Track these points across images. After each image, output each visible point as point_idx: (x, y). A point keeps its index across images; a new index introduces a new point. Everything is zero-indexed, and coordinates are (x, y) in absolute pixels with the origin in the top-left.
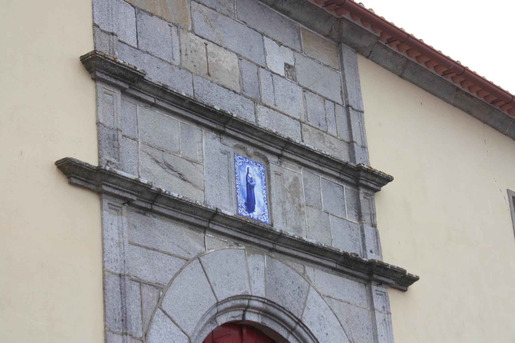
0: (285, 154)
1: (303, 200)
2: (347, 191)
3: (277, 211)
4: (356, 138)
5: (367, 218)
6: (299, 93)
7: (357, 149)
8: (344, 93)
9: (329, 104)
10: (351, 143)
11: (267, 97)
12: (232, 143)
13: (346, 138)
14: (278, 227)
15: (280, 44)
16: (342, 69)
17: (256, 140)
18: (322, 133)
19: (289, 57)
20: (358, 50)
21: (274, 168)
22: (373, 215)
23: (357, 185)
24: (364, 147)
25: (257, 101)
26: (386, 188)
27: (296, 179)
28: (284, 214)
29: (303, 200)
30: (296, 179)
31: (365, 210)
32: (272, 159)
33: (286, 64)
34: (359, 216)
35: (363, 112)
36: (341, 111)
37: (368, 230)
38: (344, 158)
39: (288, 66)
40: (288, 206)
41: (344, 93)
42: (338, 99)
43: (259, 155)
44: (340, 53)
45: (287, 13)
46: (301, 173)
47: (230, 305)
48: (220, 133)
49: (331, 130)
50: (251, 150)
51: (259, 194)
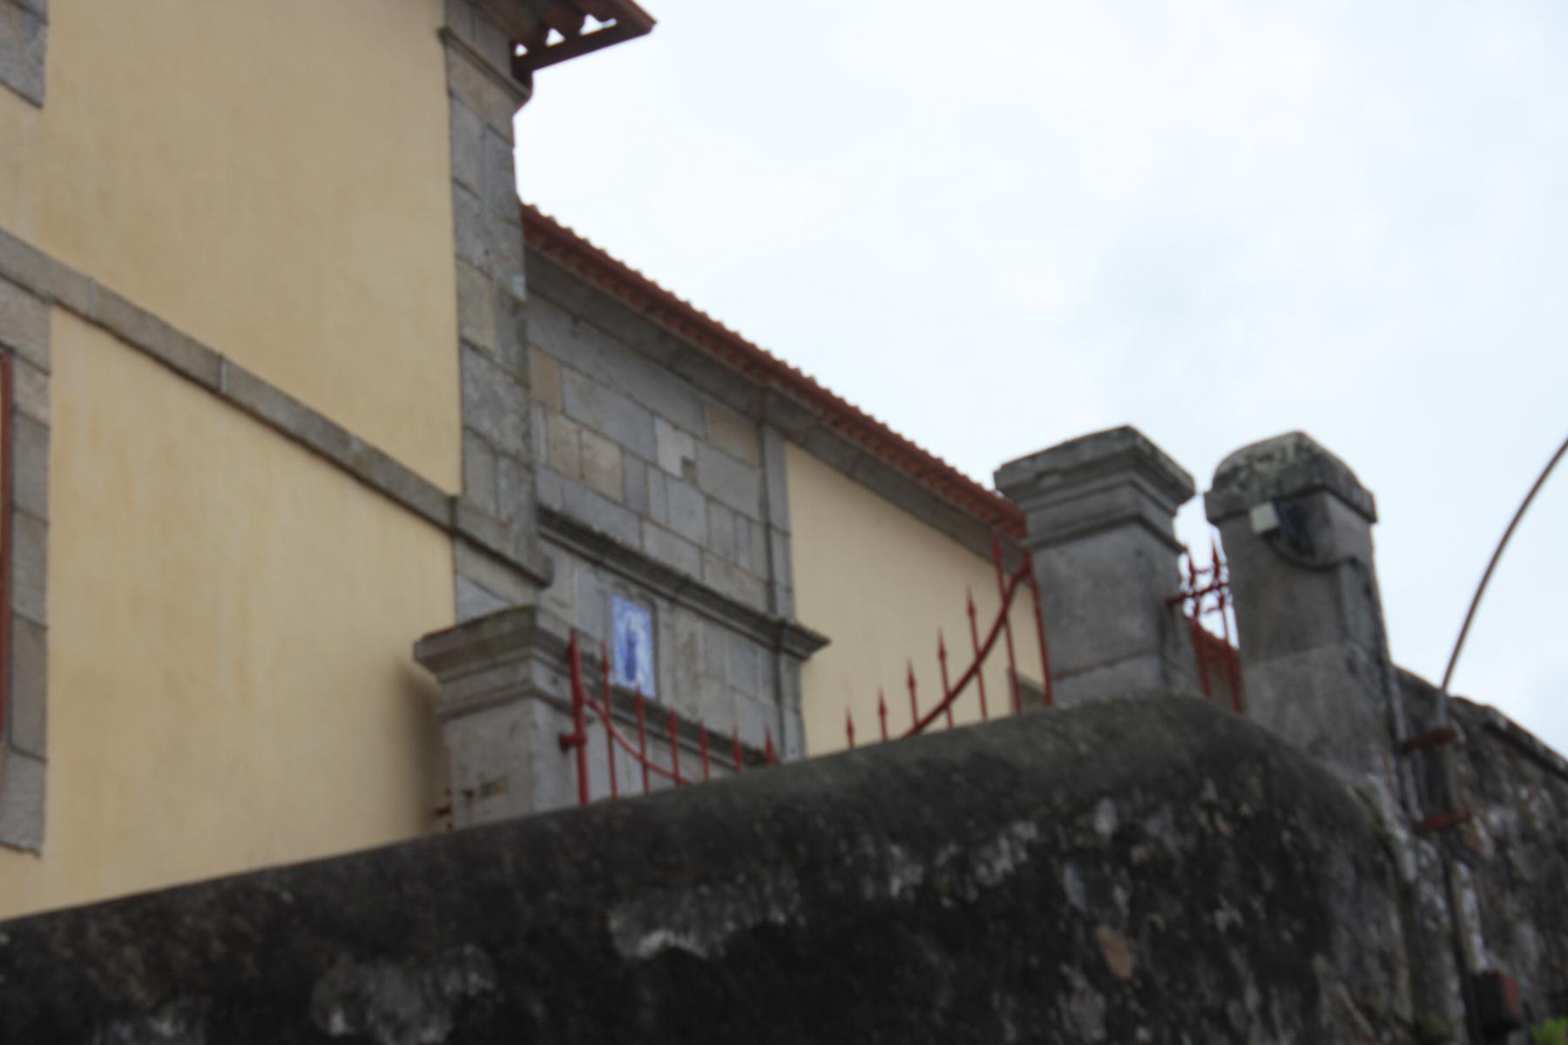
0: (682, 598)
1: (701, 666)
2: (761, 657)
3: (666, 682)
4: (779, 576)
5: (788, 700)
6: (699, 503)
7: (780, 594)
8: (764, 505)
9: (742, 522)
10: (770, 584)
11: (656, 511)
12: (610, 579)
13: (762, 572)
14: (667, 701)
15: (676, 427)
16: (763, 465)
17: (1067, 500)
18: (730, 567)
19: (687, 448)
20: (787, 435)
21: (664, 617)
22: (797, 696)
23: (776, 649)
24: (789, 590)
25: (643, 516)
26: (820, 657)
27: (692, 636)
28: (675, 685)
29: (701, 666)
30: (692, 636)
31: (786, 678)
32: (662, 604)
33: (37, 105)
34: (778, 695)
35: (46, 372)
36: (758, 534)
37: (789, 718)
38: (760, 606)
39: (687, 464)
40: (681, 675)
41: (764, 505)
42: (754, 511)
43: (642, 597)
44: (761, 441)
45: (688, 379)
46: (700, 627)
47: (631, 784)
48: (597, 564)
49: (744, 562)
50: (634, 590)
51: (643, 655)
